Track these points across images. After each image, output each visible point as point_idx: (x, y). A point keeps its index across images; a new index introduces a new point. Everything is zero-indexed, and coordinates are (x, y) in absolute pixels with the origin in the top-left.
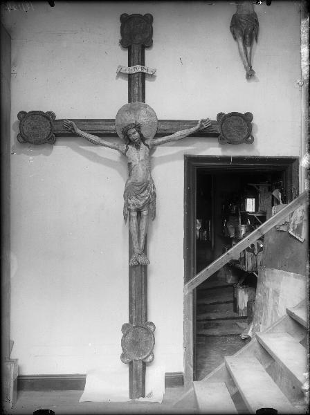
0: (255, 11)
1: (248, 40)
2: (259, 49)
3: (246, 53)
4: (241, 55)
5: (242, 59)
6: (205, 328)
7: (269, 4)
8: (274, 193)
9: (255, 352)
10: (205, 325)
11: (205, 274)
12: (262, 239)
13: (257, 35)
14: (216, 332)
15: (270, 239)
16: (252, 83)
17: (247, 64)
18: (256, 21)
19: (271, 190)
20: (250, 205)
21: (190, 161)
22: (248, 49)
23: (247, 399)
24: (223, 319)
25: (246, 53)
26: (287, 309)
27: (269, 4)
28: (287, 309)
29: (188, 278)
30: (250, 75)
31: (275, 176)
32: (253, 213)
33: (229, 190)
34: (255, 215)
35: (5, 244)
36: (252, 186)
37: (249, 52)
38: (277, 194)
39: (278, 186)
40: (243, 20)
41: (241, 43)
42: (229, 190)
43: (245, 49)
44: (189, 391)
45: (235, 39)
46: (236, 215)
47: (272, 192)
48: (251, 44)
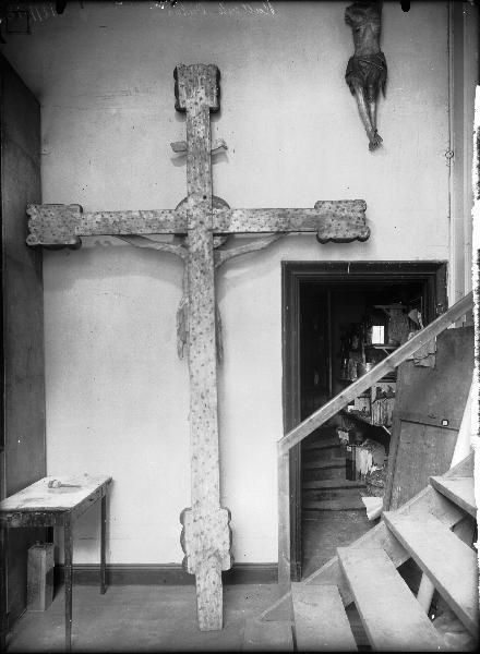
0: (383, 50)
1: (371, 92)
2: (387, 107)
3: (369, 113)
4: (361, 114)
5: (364, 122)
6: (320, 500)
7: (406, 8)
8: (411, 315)
9: (383, 542)
10: (318, 495)
11: (307, 427)
12: (391, 377)
13: (384, 83)
14: (333, 505)
15: (406, 378)
16: (378, 155)
17: (370, 128)
18: (385, 66)
19: (406, 312)
20: (378, 335)
21: (289, 269)
22: (372, 105)
23: (371, 631)
24: (342, 488)
25: (369, 113)
26: (109, 482)
27: (406, 8)
28: (109, 482)
29: (288, 428)
30: (375, 142)
31: (412, 289)
32: (381, 345)
33: (348, 309)
34: (384, 348)
35: (17, 363)
36: (380, 310)
37: (373, 110)
38: (418, 316)
39: (416, 305)
40: (363, 64)
41: (361, 97)
42: (348, 309)
43: (368, 106)
44: (285, 598)
45: (353, 92)
46: (359, 350)
47: (408, 313)
48: (376, 98)
